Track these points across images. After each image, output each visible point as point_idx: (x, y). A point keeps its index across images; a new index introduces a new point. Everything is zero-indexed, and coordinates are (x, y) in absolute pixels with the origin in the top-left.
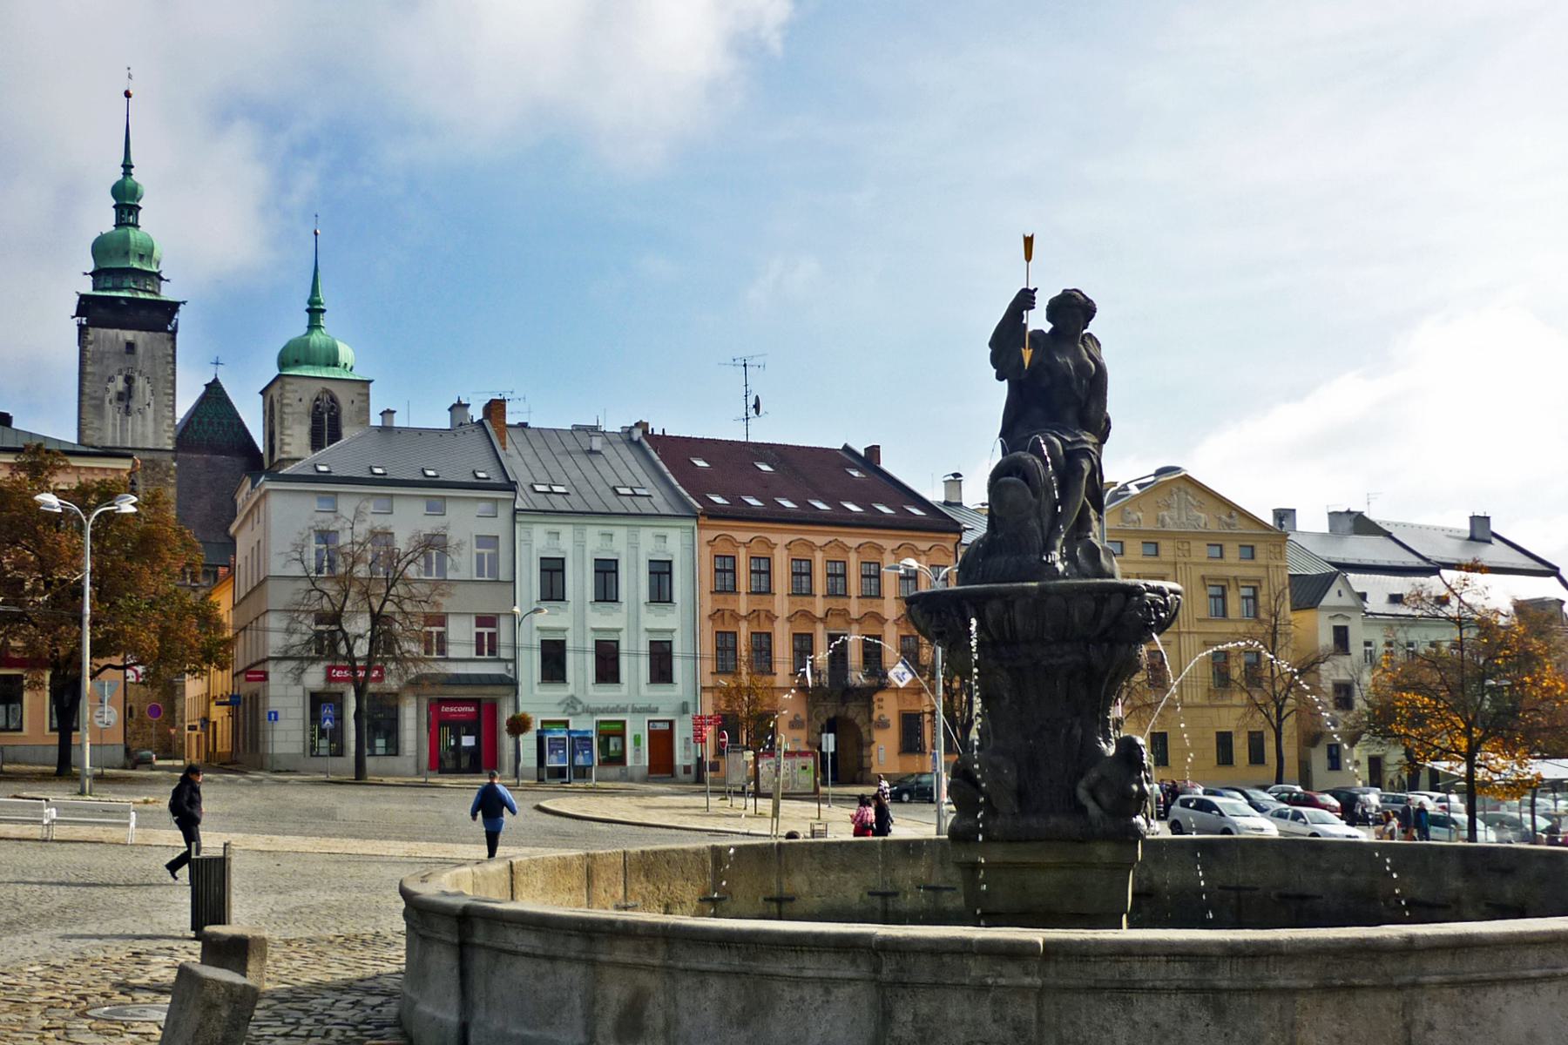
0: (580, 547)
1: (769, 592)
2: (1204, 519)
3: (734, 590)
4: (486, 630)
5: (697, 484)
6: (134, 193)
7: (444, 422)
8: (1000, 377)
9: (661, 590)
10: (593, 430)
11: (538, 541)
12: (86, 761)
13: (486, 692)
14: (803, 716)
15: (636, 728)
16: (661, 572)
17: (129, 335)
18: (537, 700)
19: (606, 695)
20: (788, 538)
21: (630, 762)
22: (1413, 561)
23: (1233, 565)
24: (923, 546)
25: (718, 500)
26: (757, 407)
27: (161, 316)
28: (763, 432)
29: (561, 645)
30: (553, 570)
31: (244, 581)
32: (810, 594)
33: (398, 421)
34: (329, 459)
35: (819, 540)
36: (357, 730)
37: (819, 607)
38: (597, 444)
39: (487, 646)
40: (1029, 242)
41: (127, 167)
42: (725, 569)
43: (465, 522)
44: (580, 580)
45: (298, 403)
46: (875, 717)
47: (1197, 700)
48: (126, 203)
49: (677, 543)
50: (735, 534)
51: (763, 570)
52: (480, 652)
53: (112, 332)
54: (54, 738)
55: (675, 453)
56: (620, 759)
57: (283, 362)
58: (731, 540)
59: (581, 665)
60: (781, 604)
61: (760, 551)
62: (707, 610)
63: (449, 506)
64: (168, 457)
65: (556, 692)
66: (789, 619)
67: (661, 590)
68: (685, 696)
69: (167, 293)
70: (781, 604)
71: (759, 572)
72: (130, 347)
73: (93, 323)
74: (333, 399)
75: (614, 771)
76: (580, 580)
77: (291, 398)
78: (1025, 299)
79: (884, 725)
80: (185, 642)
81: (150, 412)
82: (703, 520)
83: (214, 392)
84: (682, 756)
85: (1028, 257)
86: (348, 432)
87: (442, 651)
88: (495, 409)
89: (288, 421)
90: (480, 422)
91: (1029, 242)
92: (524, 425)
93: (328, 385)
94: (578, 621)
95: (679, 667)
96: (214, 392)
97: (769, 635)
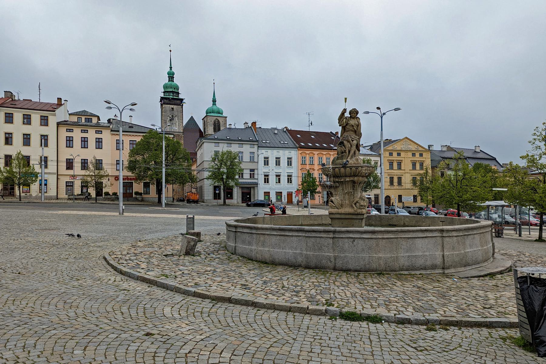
0: (272, 154)
2: (413, 147)
5: (297, 141)
6: (173, 74)
7: (243, 127)
9: (290, 163)
10: (276, 129)
11: (264, 153)
12: (164, 201)
15: (285, 194)
17: (172, 106)
19: (278, 186)
22: (489, 157)
23: (417, 158)
25: (302, 144)
26: (311, 123)
27: (180, 102)
28: (312, 129)
29: (401, 195)
31: (199, 162)
33: (233, 127)
34: (218, 135)
35: (324, 153)
36: (223, 193)
38: (276, 132)
39: (252, 176)
40: (346, 99)
41: (171, 68)
43: (246, 150)
44: (272, 162)
45: (211, 121)
47: (409, 187)
48: (171, 77)
49: (294, 154)
52: (251, 177)
54: (157, 196)
55: (293, 133)
57: (207, 113)
58: (305, 153)
64: (181, 134)
65: (267, 185)
67: (290, 163)
69: (181, 97)
73: (164, 103)
74: (218, 121)
76: (272, 162)
77: (209, 120)
78: (345, 110)
80: (182, 178)
81: (177, 124)
84: (295, 200)
85: (346, 102)
86: (222, 128)
87: (242, 177)
88: (254, 124)
89: (209, 126)
90: (251, 127)
91: (346, 99)
93: (218, 118)
95: (294, 179)
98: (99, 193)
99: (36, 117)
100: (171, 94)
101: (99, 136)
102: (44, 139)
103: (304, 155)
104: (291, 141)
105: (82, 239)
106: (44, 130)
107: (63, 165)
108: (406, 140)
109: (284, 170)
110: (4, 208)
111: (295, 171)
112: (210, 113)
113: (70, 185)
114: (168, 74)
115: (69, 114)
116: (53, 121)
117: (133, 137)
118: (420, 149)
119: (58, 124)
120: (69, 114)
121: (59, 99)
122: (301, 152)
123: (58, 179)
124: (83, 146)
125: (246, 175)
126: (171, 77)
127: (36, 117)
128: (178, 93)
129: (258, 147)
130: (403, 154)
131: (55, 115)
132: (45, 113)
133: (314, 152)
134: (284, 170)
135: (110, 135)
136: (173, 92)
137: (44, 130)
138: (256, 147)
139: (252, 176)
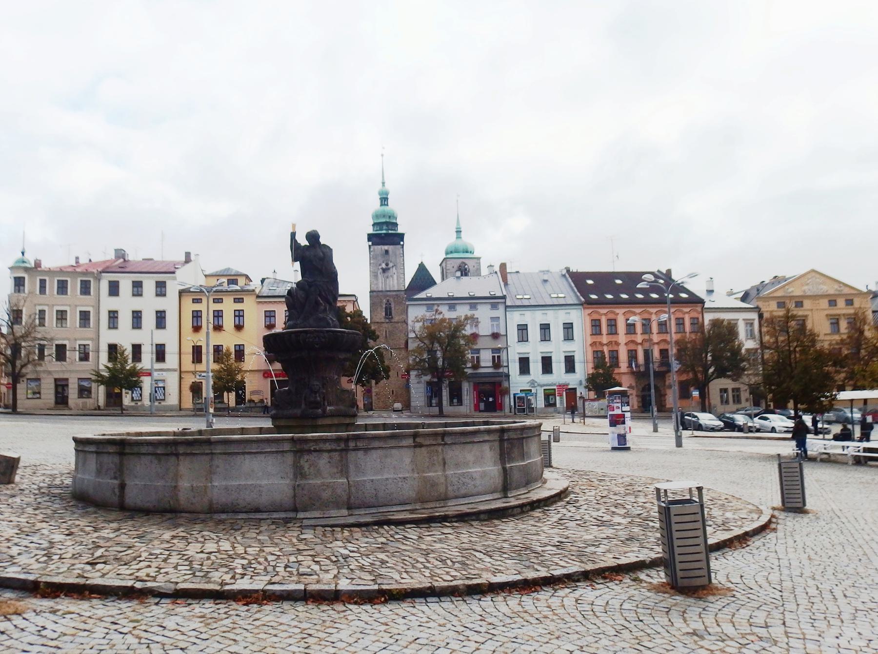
0: (533, 320)
1: (616, 333)
2: (831, 289)
3: (600, 334)
4: (496, 355)
8: (295, 260)
11: (516, 318)
13: (498, 379)
14: (634, 384)
16: (568, 327)
17: (386, 247)
18: (517, 383)
19: (547, 379)
20: (623, 310)
21: (558, 405)
24: (638, 310)
30: (523, 329)
32: (635, 333)
37: (639, 338)
39: (497, 363)
42: (596, 325)
44: (534, 333)
46: (667, 383)
48: (384, 200)
50: (599, 310)
51: (612, 325)
53: (379, 247)
56: (554, 405)
57: (447, 253)
59: (536, 367)
60: (622, 338)
61: (611, 316)
62: (589, 342)
63: (479, 307)
64: (403, 293)
65: (526, 379)
66: (626, 344)
68: (577, 379)
69: (400, 230)
70: (622, 338)
71: (595, 326)
72: (387, 252)
75: (551, 409)
76: (534, 333)
79: (670, 387)
81: (395, 277)
82: (585, 306)
83: (422, 268)
92: (518, 272)
93: (464, 260)
94: (535, 349)
95: (578, 366)
96: (422, 268)
97: (617, 351)
98: (240, 399)
99: (149, 286)
100: (385, 227)
101: (239, 306)
102: (161, 319)
103: (596, 317)
104: (572, 294)
105: (741, 573)
106: (161, 304)
107: (188, 358)
108: (813, 274)
109: (558, 349)
110: (41, 422)
111: (580, 348)
112: (451, 252)
113: (196, 389)
114: (380, 194)
115: (206, 276)
116: (173, 289)
117: (271, 305)
118: (846, 291)
119: (181, 293)
120: (206, 276)
121: (188, 255)
122: (590, 311)
123: (181, 378)
124: (111, 326)
125: (486, 358)
126: (384, 200)
127: (149, 286)
128: (396, 225)
129: (506, 307)
130: (807, 304)
131: (175, 279)
132: (161, 277)
133: (617, 311)
134: (558, 349)
135: (255, 304)
136: (387, 223)
137: (161, 304)
138: (501, 308)
139: (497, 363)
